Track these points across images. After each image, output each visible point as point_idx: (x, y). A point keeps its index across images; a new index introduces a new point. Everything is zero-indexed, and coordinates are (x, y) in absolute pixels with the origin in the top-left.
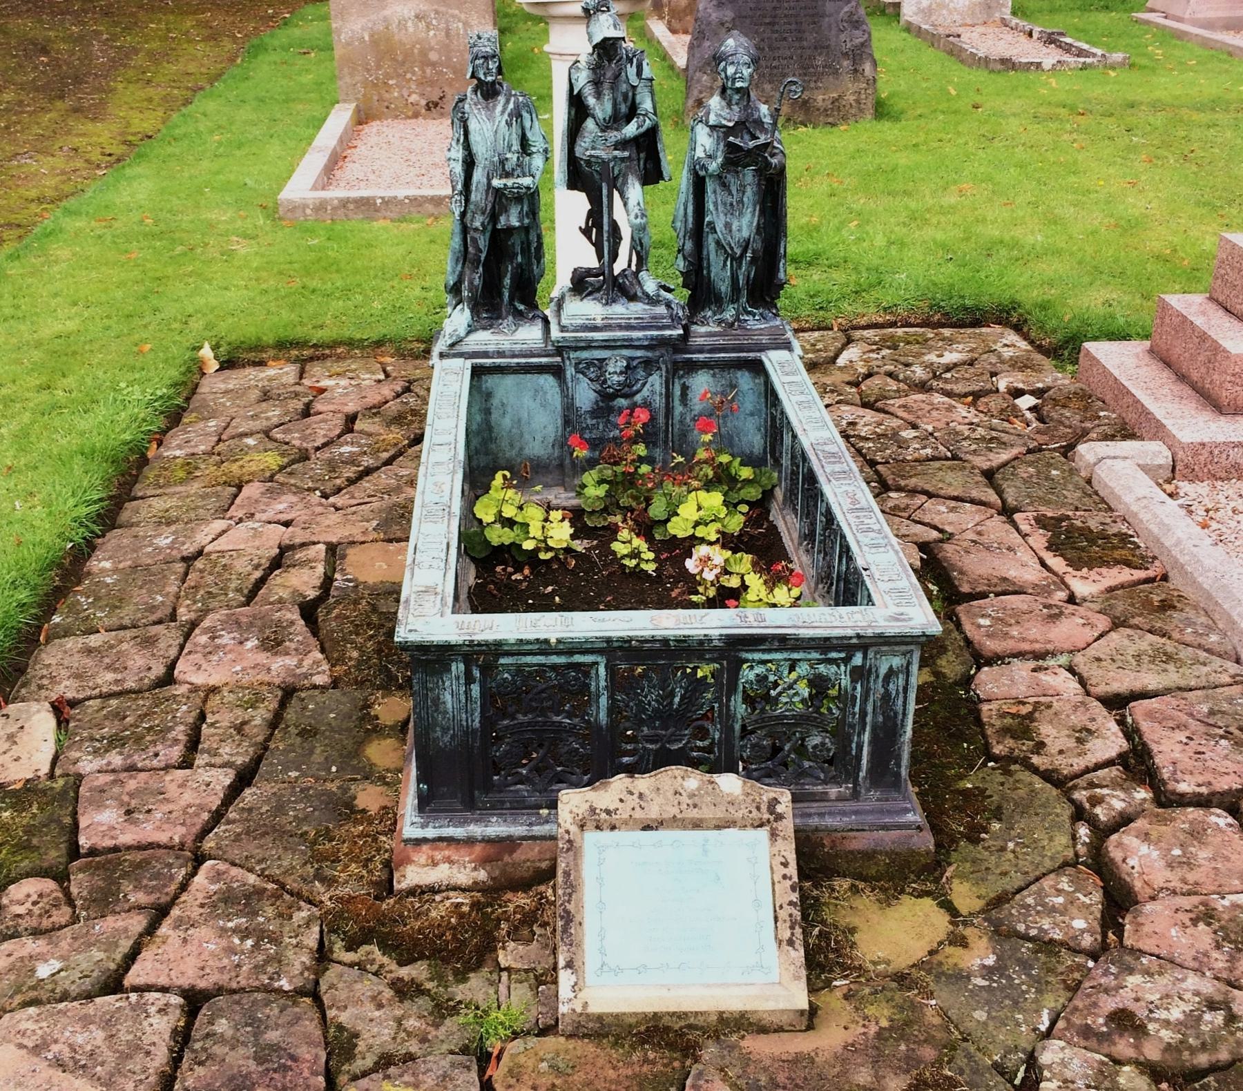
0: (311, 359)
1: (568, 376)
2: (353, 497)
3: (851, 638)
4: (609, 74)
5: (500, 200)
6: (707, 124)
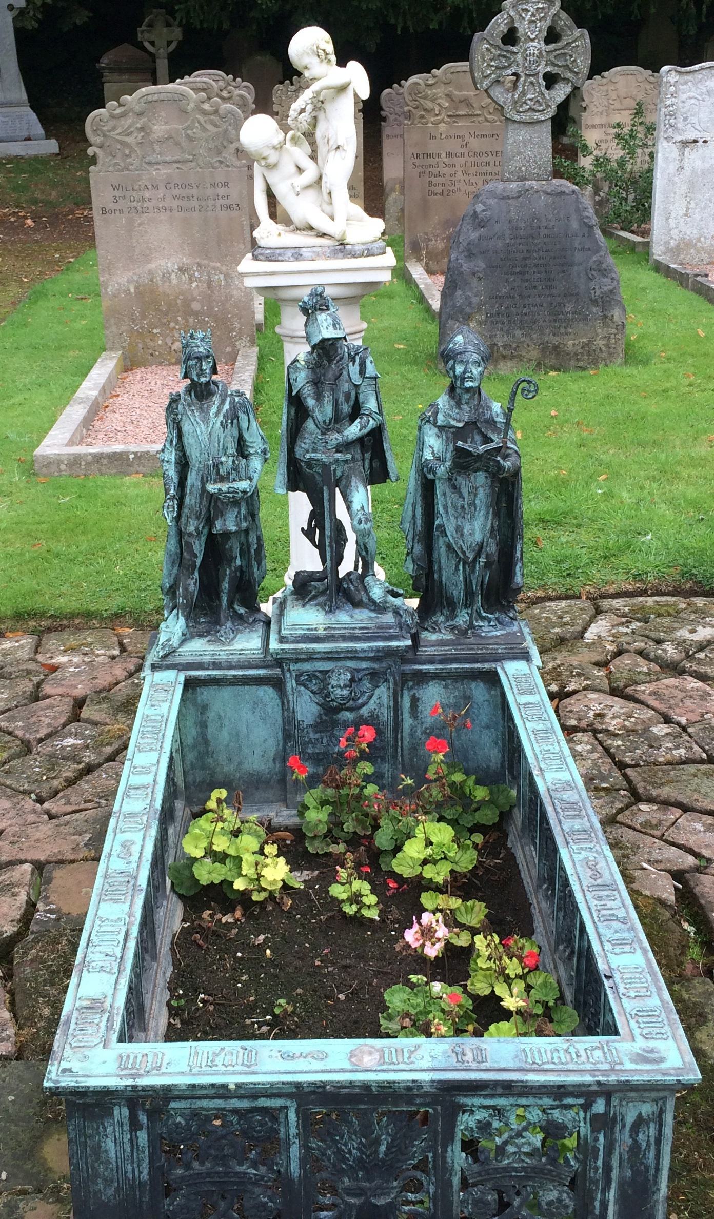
0: (49, 630)
1: (289, 688)
2: (68, 803)
3: (590, 1085)
4: (330, 374)
5: (214, 506)
6: (435, 424)
